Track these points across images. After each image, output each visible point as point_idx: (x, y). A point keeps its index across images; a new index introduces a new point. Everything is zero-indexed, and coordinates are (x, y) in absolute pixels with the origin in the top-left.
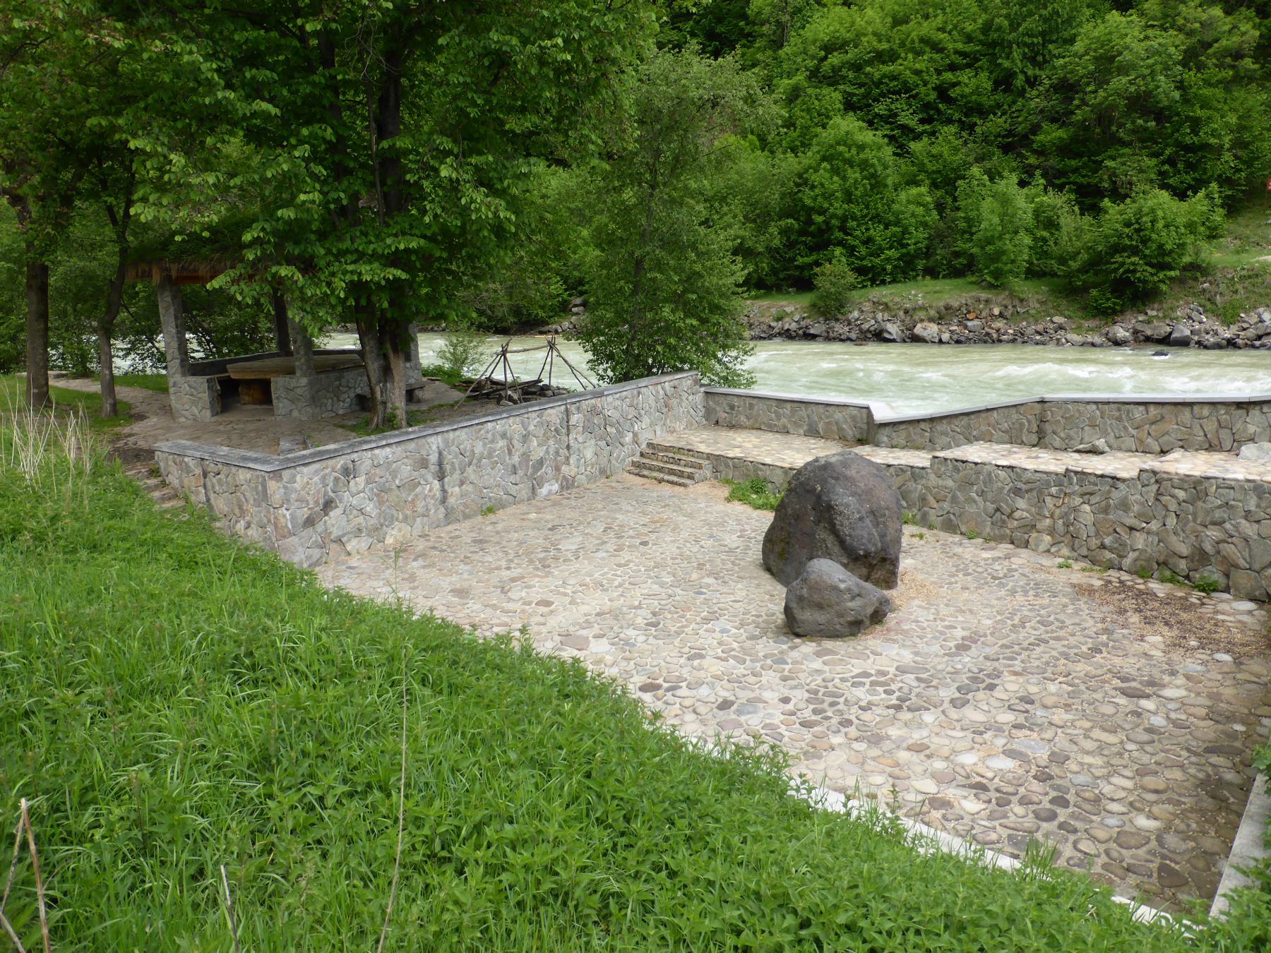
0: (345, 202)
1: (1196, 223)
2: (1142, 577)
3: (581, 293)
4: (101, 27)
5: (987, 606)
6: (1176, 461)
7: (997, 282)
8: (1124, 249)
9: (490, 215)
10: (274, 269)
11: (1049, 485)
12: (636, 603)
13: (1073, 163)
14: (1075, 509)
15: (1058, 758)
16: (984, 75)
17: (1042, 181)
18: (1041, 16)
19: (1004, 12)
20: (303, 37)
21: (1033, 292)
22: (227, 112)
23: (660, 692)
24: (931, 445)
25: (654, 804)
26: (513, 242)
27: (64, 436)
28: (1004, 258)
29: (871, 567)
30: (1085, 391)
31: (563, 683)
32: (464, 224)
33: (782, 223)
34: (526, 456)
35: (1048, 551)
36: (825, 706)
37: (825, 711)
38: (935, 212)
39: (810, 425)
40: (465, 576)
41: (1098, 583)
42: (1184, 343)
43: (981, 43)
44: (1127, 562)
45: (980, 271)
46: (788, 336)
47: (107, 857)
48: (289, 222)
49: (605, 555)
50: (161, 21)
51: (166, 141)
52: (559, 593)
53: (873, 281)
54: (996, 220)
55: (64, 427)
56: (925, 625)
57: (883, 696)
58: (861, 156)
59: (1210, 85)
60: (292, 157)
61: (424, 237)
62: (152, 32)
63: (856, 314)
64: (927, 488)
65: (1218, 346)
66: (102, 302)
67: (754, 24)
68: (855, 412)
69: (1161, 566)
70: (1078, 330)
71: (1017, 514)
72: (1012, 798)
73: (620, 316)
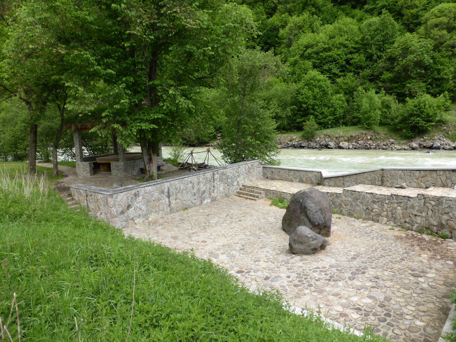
0: (137, 102)
1: (440, 105)
2: (420, 233)
3: (221, 132)
4: (58, 47)
5: (363, 243)
6: (431, 191)
7: (369, 127)
8: (415, 115)
9: (186, 106)
10: (112, 125)
11: (385, 200)
12: (237, 242)
13: (395, 85)
14: (395, 208)
15: (388, 299)
16: (362, 55)
17: (384, 92)
18: (382, 35)
19: (369, 34)
20: (124, 48)
21: (382, 131)
22: (98, 73)
23: (244, 274)
24: (343, 185)
25: (230, 308)
26: (195, 115)
27: (40, 182)
28: (371, 119)
29: (321, 229)
30: (414, 166)
31: (204, 268)
32: (177, 109)
33: (291, 107)
34: (199, 190)
35: (386, 224)
36: (303, 279)
37: (303, 281)
38: (346, 103)
39: (300, 178)
40: (176, 232)
41: (404, 235)
42: (438, 148)
43: (361, 44)
44: (414, 228)
45: (363, 123)
46: (294, 147)
47: (43, 321)
48: (118, 109)
49: (226, 225)
50: (77, 44)
51: (77, 83)
52: (209, 238)
53: (324, 127)
54: (368, 105)
55: (39, 179)
56: (340, 250)
57: (324, 276)
58: (319, 84)
59: (443, 57)
60: (119, 88)
61: (163, 114)
62: (73, 47)
63: (318, 139)
64: (342, 201)
65: (450, 149)
66: (55, 137)
67: (281, 39)
68: (316, 174)
69: (427, 229)
70: (399, 144)
71: (374, 210)
72: (370, 313)
73: (233, 141)
